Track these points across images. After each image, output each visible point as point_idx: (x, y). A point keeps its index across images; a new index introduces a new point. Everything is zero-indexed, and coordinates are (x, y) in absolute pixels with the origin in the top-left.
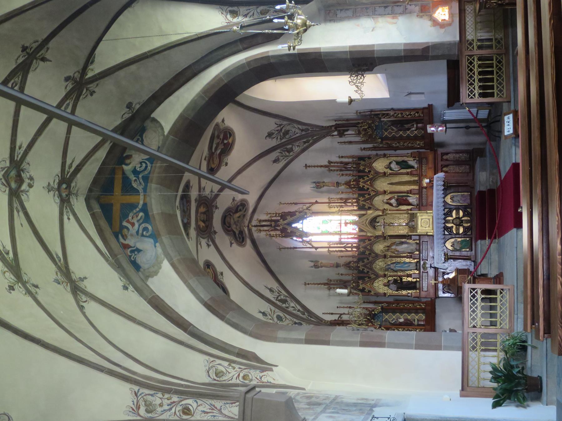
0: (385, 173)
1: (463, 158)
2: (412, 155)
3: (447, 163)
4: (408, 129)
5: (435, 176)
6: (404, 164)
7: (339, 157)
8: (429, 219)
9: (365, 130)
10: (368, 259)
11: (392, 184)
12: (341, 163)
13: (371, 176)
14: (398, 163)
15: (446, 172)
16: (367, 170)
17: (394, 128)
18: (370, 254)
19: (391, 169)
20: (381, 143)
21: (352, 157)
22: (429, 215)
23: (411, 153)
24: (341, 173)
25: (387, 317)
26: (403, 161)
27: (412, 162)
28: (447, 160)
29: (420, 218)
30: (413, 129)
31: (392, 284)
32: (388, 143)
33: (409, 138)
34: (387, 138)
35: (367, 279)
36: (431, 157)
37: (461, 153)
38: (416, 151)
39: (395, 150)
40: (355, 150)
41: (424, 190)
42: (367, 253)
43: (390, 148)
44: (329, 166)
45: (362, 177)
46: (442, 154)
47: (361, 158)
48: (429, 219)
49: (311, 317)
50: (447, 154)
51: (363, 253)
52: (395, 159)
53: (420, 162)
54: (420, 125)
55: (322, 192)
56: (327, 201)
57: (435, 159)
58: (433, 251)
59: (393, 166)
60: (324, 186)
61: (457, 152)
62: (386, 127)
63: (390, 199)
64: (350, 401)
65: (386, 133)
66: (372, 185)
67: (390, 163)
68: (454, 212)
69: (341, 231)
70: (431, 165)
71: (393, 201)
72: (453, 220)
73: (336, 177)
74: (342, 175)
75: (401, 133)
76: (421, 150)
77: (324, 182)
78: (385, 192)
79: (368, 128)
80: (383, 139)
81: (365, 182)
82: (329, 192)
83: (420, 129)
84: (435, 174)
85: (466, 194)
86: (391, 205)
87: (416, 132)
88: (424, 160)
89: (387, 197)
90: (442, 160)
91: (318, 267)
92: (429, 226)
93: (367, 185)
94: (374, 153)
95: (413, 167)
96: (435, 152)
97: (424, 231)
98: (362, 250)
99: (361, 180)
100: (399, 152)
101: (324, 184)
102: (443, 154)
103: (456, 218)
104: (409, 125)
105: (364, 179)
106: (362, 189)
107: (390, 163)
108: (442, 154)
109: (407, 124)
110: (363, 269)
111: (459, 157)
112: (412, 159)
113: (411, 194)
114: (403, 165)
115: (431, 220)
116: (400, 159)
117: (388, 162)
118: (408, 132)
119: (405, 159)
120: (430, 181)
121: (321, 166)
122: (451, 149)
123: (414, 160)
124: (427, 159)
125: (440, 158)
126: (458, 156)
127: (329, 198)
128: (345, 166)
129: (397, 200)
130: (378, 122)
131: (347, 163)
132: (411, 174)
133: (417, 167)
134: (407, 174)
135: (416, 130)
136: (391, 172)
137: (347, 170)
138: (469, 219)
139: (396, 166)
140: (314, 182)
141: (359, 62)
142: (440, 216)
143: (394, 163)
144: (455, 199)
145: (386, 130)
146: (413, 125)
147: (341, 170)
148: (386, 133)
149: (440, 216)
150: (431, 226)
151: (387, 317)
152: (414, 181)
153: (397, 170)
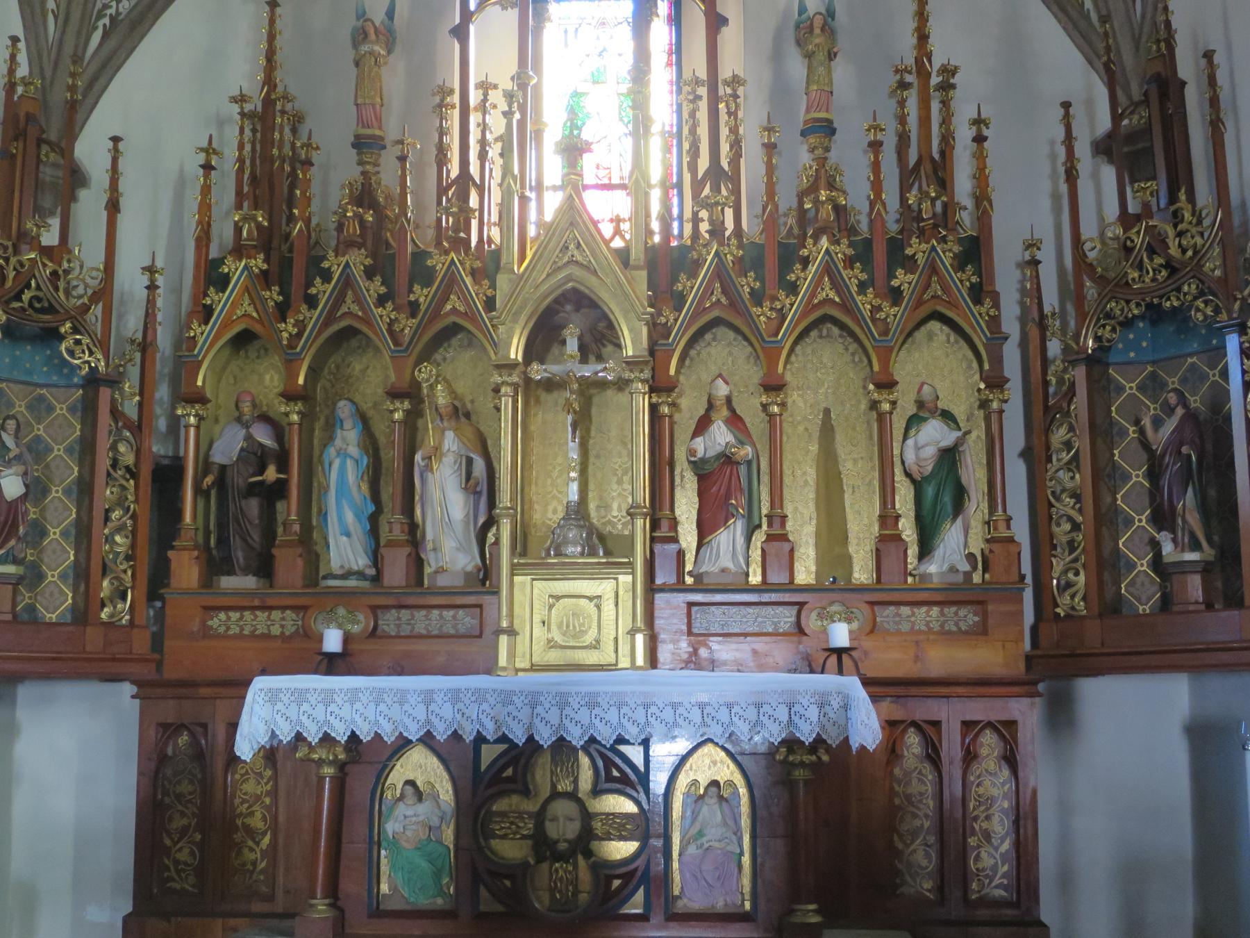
0: (887, 384)
1: (987, 861)
2: (1000, 542)
3: (953, 770)
4: (1163, 518)
5: (853, 684)
6: (947, 499)
7: (978, 122)
8: (596, 645)
9: (1156, 246)
10: (381, 301)
11: (827, 430)
12: (947, 139)
13: (864, 303)
14: (949, 457)
15: (892, 749)
16: (902, 278)
17: (1171, 425)
18: (414, 308)
19: (914, 421)
20: (1072, 356)
21: (982, 198)
22: (624, 649)
23: (1011, 540)
24: (890, 141)
25: (61, 409)
26: (960, 495)
27: (957, 544)
28: (970, 756)
29: (604, 588)
30: (1167, 548)
31: (249, 438)
32: (1071, 393)
33: (1107, 519)
34: (1101, 388)
35: (273, 295)
36: (988, 658)
37: (1017, 844)
38: (1027, 568)
39: (1027, 454)
40: (1024, 218)
41: (786, 617)
42: (422, 295)
43: (1044, 411)
44: (925, 79)
45: (862, 254)
46: (1011, 724)
47: (975, 252)
48: (596, 645)
49: (106, 35)
50: (1010, 759)
51: (422, 274)
52: (978, 435)
53: (954, 595)
54: (1194, 587)
55: (777, 57)
56: (725, 72)
57: (981, 684)
58: (740, 667)
59: (934, 435)
60: (809, 56)
61: (1024, 819)
62: (1173, 382)
63: (735, 421)
64: (269, 427)
65: (1131, 387)
66: (819, 322)
67: (948, 417)
68: (629, 807)
69: (586, 187)
70: (941, 660)
71: (720, 436)
72: (573, 796)
73: (859, 98)
74: (876, 146)
75: (1138, 477)
76: (1028, 595)
77: (831, 56)
78: (774, 386)
79: (1171, 266)
80: (1096, 362)
81: (828, 269)
82: (779, 92)
83: (1162, 587)
84: (867, 682)
85: (746, 882)
86: (703, 425)
87: (1143, 566)
88: (969, 617)
89: (750, 407)
90: (967, 725)
91: (355, 45)
92: (552, 645)
93: (818, 283)
94: (1011, 326)
95: (925, 550)
96: (1022, 685)
97: (521, 610)
98: (438, 262)
99: (843, 250)
100: (1016, 472)
101: (821, 56)
102: (1007, 730)
103: (587, 816)
104: (1194, 520)
105: (850, 262)
106: (790, 256)
107: (948, 417)
108: (1011, 724)
109: (1203, 507)
110: (326, 276)
111: (987, 836)
112: (976, 546)
113: (770, 538)
114: (942, 491)
115: (592, 658)
116: (974, 474)
117: (960, 412)
118: (1142, 520)
119: (977, 506)
120: (840, 652)
121: (923, 37)
122: (1040, 774)
123: (971, 557)
124: (982, 631)
125: (978, 710)
126: (1000, 825)
127: (735, 81)
128: (927, 167)
129: (727, 459)
130: (1209, 323)
131: (944, 184)
132: (888, 540)
133: (924, 577)
134: (888, 518)
135: (1157, 563)
136: (898, 425)
137: (908, 177)
138: (583, 897)
139: (930, 452)
140: (831, 13)
141: (1183, 535)
142: (584, 716)
143: (949, 438)
144: (712, 812)
145: (1153, 386)
146: (1195, 545)
147: (903, 139)
148: (1131, 387)
149: (584, 716)
150: (554, 657)
151: (61, 409)
152: (847, 561)
153: (910, 457)
